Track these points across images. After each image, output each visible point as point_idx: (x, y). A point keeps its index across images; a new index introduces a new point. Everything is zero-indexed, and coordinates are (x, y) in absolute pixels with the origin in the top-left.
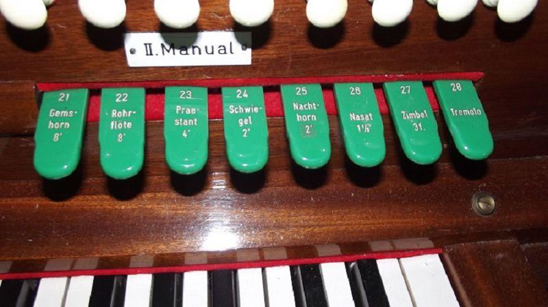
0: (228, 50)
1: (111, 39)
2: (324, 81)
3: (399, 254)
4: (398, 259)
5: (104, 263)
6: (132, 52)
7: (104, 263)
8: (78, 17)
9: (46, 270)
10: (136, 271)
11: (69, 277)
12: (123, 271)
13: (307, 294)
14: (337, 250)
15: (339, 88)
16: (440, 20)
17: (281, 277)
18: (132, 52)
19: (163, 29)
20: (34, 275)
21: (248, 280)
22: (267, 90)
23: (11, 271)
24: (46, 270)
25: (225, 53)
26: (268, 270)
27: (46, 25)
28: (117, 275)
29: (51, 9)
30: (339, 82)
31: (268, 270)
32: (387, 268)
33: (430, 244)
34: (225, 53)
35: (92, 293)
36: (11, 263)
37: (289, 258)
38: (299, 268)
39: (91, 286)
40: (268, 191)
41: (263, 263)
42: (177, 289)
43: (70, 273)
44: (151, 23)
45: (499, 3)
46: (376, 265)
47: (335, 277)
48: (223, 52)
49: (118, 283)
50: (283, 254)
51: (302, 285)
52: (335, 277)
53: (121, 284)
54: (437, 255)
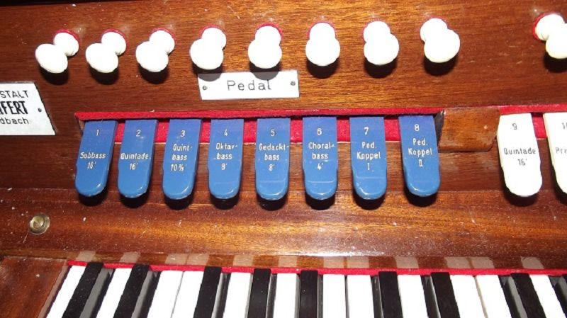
0: (266, 87)
3: (474, 272)
4: (474, 276)
6: (293, 84)
8: (299, 54)
9: (120, 261)
12: (159, 267)
13: (253, 297)
15: (548, 117)
17: (362, 287)
19: (253, 69)
21: (332, 285)
22: (534, 115)
24: (120, 261)
25: (264, 89)
26: (349, 277)
27: (66, 71)
29: (71, 59)
31: (349, 277)
34: (264, 89)
41: (346, 272)
42: (432, 296)
47: (411, 290)
48: (262, 88)
50: (366, 265)
52: (411, 290)
53: (156, 276)
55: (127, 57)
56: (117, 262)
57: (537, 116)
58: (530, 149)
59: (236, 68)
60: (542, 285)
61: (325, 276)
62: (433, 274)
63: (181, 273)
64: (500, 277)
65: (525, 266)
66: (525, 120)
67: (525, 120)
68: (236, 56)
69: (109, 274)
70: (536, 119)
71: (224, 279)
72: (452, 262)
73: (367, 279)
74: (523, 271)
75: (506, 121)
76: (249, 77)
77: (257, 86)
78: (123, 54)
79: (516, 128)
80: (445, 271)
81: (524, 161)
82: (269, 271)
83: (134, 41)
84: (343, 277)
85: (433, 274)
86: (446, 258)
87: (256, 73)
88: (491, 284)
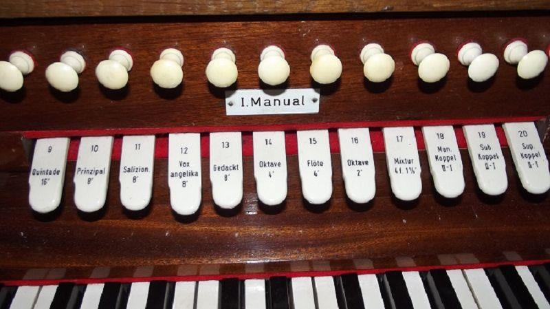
0: (300, 102)
1: (221, 93)
2: (330, 126)
3: (462, 267)
5: (159, 270)
7: (159, 270)
10: (251, 277)
11: (41, 286)
14: (329, 269)
16: (420, 80)
17: (326, 285)
18: (231, 105)
20: (81, 281)
22: (455, 127)
23: (110, 276)
24: (91, 277)
25: (270, 105)
28: (123, 283)
30: (342, 127)
32: (454, 276)
33: (476, 261)
34: (270, 105)
35: (54, 300)
36: (152, 267)
37: (481, 262)
38: (385, 276)
39: (54, 296)
40: (153, 214)
41: (313, 274)
43: (41, 283)
44: (256, 79)
45: (421, 64)
46: (357, 279)
47: (369, 285)
49: (123, 289)
50: (262, 270)
51: (166, 298)
52: (369, 285)
54: (418, 273)
55: (87, 75)
56: (20, 279)
57: (333, 134)
58: (448, 161)
59: (298, 85)
60: (524, 273)
61: (247, 282)
62: (343, 276)
63: (193, 284)
64: (377, 276)
65: (443, 262)
66: (408, 132)
67: (408, 132)
68: (248, 77)
69: (79, 292)
70: (288, 135)
71: (123, 292)
72: (444, 260)
73: (217, 283)
74: (509, 263)
75: (42, 145)
76: (258, 93)
77: (262, 102)
78: (30, 74)
79: (484, 136)
80: (353, 271)
81: (414, 169)
82: (236, 280)
83: (43, 61)
84: (310, 278)
85: (343, 276)
86: (504, 253)
87: (267, 90)
88: (478, 277)
